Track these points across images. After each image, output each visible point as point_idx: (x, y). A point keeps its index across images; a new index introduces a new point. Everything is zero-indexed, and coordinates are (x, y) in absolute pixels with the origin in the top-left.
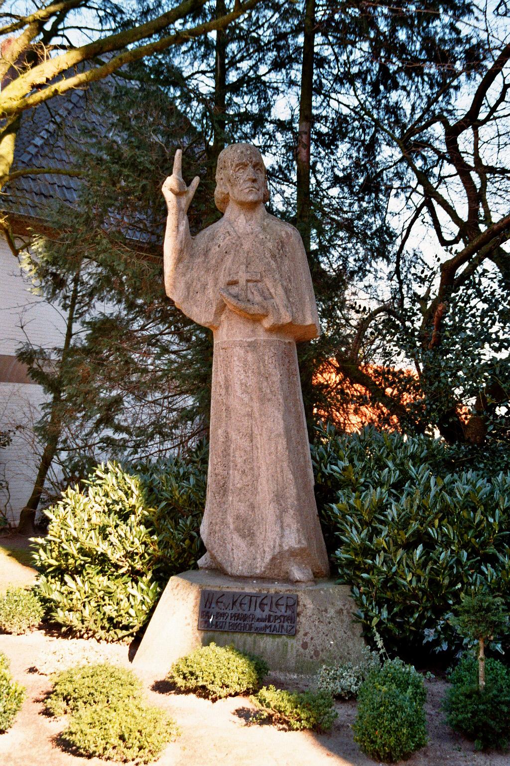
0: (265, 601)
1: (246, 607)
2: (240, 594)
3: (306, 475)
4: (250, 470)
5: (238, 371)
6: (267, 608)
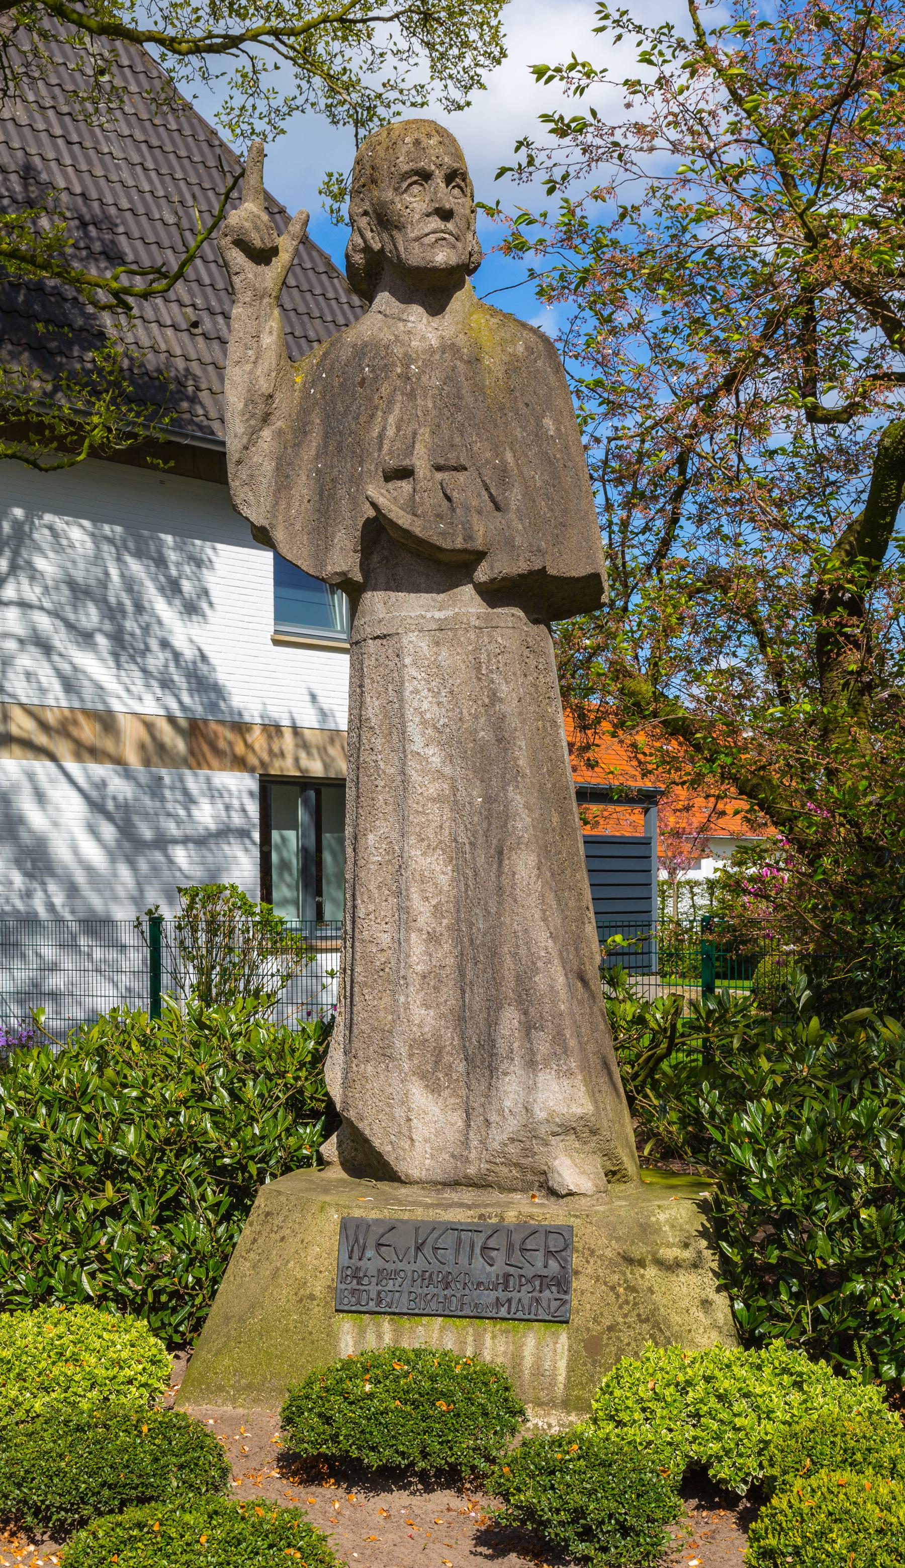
0: (492, 1243)
1: (450, 1255)
2: (434, 1226)
3: (578, 940)
4: (447, 1206)
5: (416, 692)
6: (499, 1257)
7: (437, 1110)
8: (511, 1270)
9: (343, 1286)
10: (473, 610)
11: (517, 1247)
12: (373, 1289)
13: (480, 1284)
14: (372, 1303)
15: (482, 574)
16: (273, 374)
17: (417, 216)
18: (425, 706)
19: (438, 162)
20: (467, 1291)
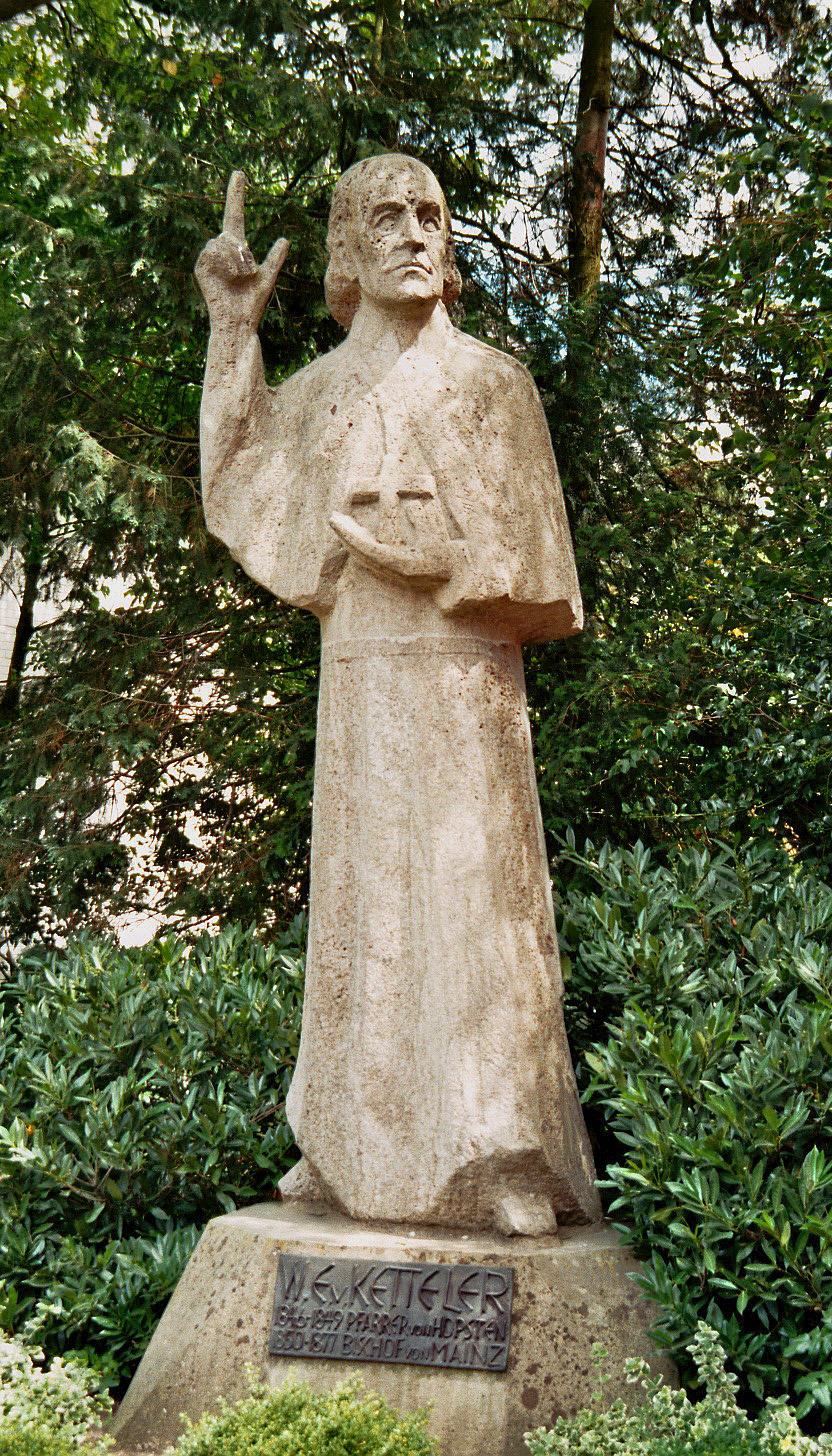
0: (433, 1285)
5: (377, 716)
6: (438, 1303)
7: (387, 1143)
8: (449, 1315)
9: (277, 1329)
10: (437, 635)
11: (455, 1290)
12: (307, 1332)
13: (417, 1328)
14: (306, 1348)
15: (448, 599)
16: (248, 399)
17: (388, 250)
18: (386, 730)
19: (412, 196)
20: (403, 1336)
